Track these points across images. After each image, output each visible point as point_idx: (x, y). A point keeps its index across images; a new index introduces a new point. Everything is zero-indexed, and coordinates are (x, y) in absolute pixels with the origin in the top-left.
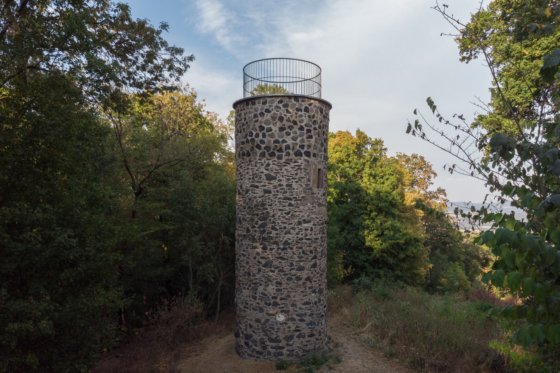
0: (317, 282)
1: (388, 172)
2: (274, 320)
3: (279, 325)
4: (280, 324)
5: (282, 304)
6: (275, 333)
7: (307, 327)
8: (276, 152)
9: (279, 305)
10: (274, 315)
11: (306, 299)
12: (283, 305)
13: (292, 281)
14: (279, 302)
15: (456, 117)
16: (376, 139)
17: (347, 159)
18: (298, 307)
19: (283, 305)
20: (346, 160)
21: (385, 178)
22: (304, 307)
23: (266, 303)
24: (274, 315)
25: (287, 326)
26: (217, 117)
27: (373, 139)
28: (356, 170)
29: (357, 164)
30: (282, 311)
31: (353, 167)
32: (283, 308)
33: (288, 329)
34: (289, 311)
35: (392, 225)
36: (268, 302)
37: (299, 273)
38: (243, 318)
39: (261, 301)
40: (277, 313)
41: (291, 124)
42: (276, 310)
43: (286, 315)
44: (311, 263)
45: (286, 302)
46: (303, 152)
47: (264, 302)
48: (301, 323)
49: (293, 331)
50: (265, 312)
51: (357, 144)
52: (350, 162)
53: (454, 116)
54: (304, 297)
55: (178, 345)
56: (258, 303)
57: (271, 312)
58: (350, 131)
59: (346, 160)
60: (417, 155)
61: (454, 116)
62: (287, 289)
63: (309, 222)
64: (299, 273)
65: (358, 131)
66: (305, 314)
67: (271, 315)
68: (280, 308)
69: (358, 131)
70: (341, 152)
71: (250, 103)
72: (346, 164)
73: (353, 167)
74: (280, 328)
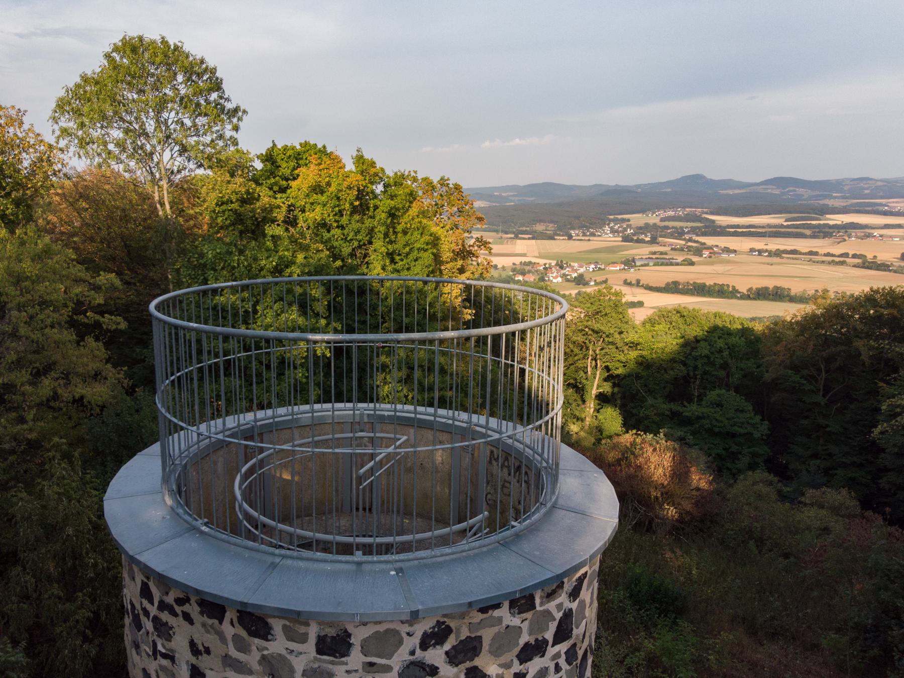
1: (417, 245)
16: (396, 174)
17: (336, 221)
20: (335, 225)
21: (411, 257)
26: (24, 119)
27: (390, 172)
28: (356, 244)
29: (358, 232)
31: (348, 239)
35: (792, 499)
42: (41, 288)
51: (358, 188)
52: (342, 227)
55: (272, 431)
58: (294, 145)
59: (335, 225)
60: (448, 179)
65: (360, 159)
69: (360, 159)
70: (324, 205)
72: (336, 232)
73: (348, 239)
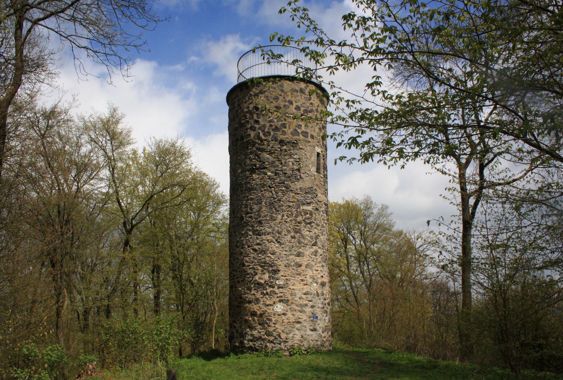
0: (319, 271)
2: (272, 311)
3: (276, 316)
4: (278, 315)
5: (281, 293)
6: (273, 325)
7: (308, 320)
8: (271, 131)
9: (277, 294)
10: (271, 305)
11: (306, 289)
12: (282, 294)
13: (291, 268)
14: (277, 291)
15: (338, 161)
18: (299, 296)
19: (282, 294)
22: (304, 296)
23: (262, 293)
24: (271, 305)
25: (286, 317)
30: (281, 301)
32: (281, 297)
33: (288, 321)
34: (288, 301)
36: (265, 292)
37: (298, 259)
38: (238, 315)
39: (257, 292)
40: (274, 303)
41: (287, 104)
43: (285, 305)
44: (312, 250)
45: (284, 291)
46: (299, 131)
47: (260, 292)
48: (301, 314)
49: (293, 322)
50: (262, 302)
53: (336, 163)
54: (305, 286)
56: (254, 294)
57: (268, 303)
61: (336, 163)
62: (285, 276)
63: (309, 204)
64: (298, 259)
66: (306, 305)
67: (268, 305)
68: (278, 297)
71: (244, 88)
74: (279, 320)
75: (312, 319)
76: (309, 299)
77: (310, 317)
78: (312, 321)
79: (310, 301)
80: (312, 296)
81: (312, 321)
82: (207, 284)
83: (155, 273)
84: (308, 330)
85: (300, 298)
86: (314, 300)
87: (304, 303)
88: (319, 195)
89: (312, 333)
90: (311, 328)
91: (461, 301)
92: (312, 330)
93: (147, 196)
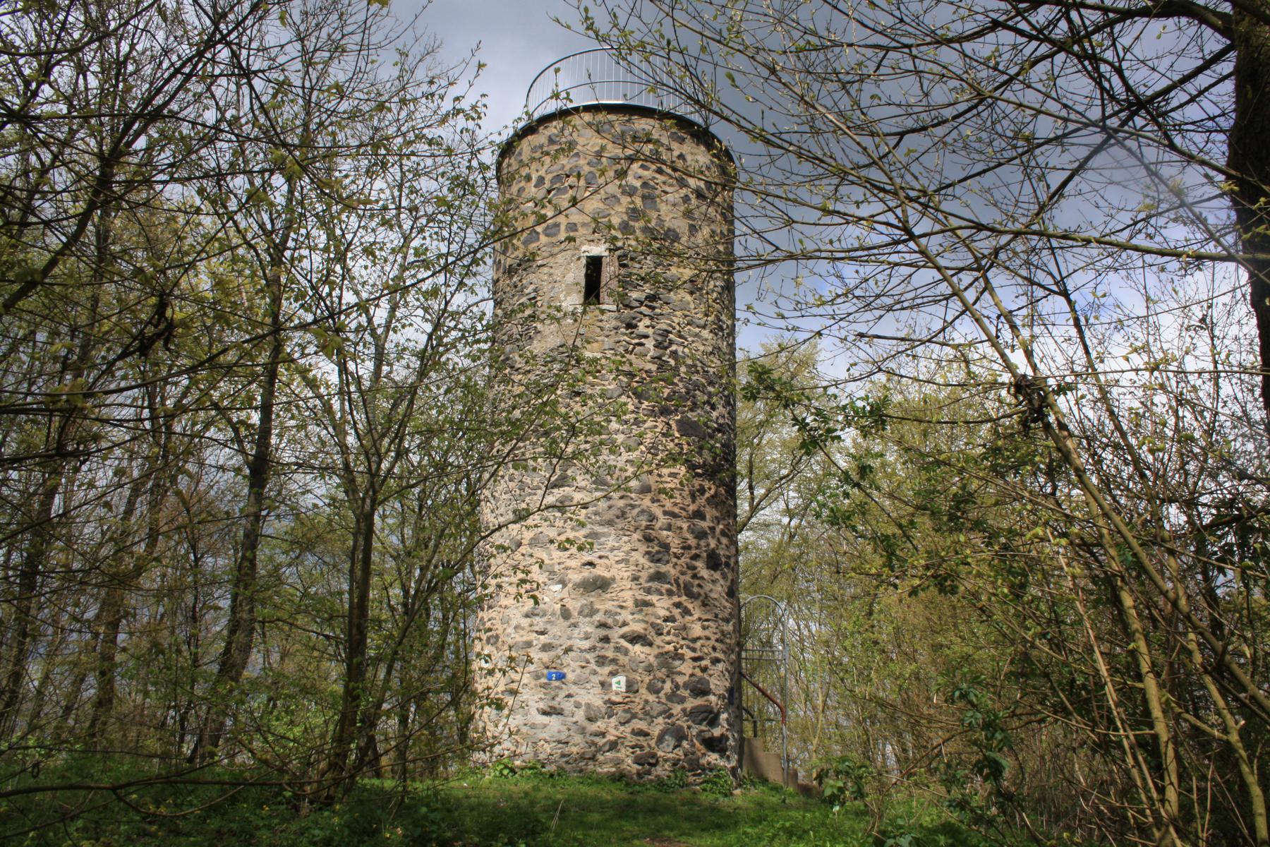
7: (533, 683)
18: (514, 623)
75: (544, 680)
76: (536, 628)
77: (537, 677)
78: (543, 686)
79: (543, 633)
80: (545, 619)
81: (543, 686)
82: (377, 143)
83: (609, 305)
84: (534, 712)
85: (516, 628)
86: (553, 630)
87: (525, 639)
88: (688, 298)
89: (545, 719)
90: (542, 705)
91: (1240, 745)
92: (545, 713)
93: (724, 698)
